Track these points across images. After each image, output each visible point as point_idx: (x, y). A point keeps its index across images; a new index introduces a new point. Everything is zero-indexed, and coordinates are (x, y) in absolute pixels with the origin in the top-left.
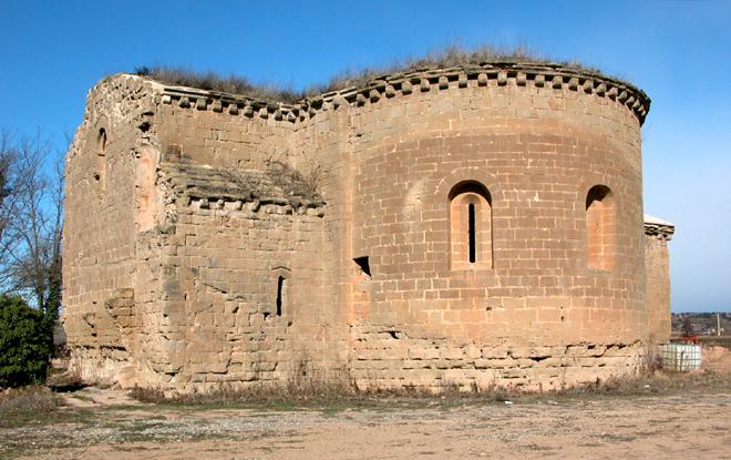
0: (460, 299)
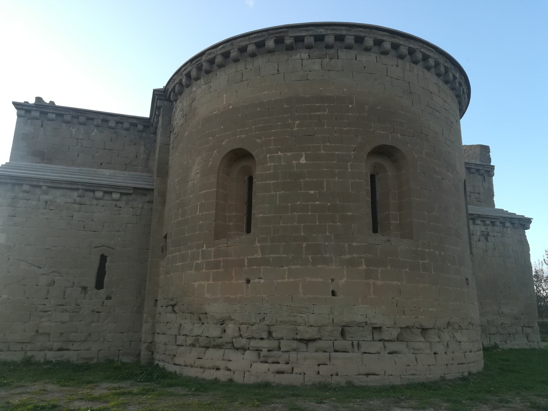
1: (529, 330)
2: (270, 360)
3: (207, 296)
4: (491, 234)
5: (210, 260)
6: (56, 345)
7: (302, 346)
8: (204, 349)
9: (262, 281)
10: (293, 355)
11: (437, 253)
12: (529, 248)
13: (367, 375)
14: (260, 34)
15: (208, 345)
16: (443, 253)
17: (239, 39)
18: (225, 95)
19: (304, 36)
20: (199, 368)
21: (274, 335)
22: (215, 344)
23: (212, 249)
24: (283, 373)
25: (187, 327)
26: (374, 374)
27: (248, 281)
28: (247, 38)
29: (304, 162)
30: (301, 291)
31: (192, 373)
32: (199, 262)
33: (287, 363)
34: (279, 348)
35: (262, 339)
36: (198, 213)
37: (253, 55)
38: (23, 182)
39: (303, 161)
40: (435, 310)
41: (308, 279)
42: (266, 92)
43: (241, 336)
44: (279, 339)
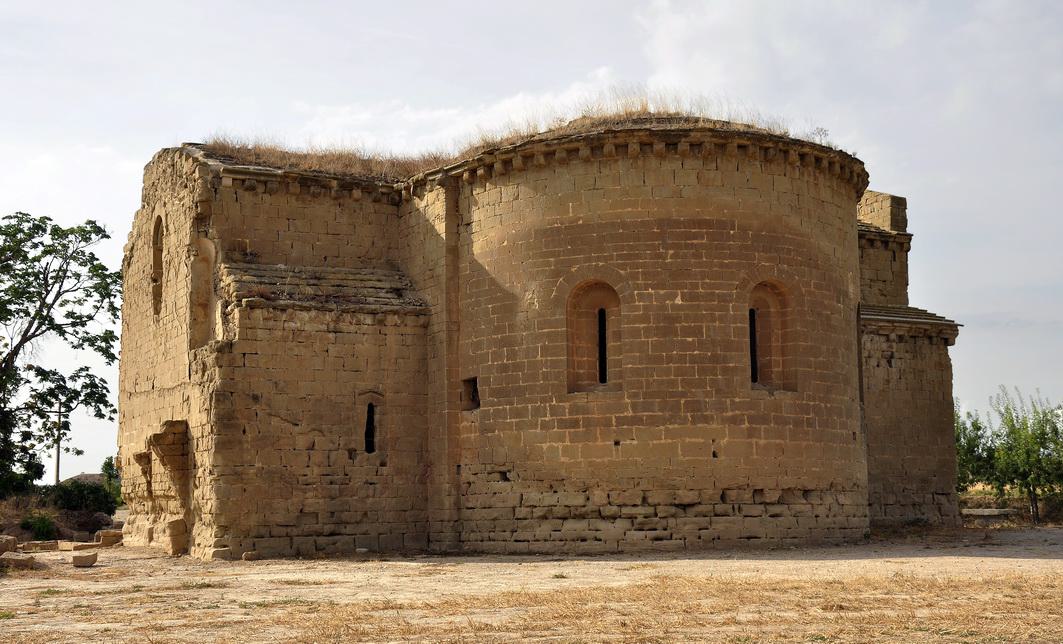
1: (943, 499)
2: (646, 527)
4: (896, 355)
6: (328, 528)
7: (680, 511)
8: (561, 521)
9: (635, 442)
10: (672, 521)
11: (823, 405)
12: (952, 375)
13: (749, 538)
15: (568, 515)
16: (829, 405)
21: (650, 500)
22: (577, 513)
23: (567, 405)
24: (661, 539)
26: (756, 538)
27: (617, 443)
29: (680, 303)
30: (680, 452)
32: (547, 419)
33: (665, 529)
34: (656, 515)
35: (635, 506)
36: (539, 358)
39: (678, 301)
40: (818, 469)
41: (688, 440)
42: (630, 209)
43: (609, 503)
44: (655, 506)
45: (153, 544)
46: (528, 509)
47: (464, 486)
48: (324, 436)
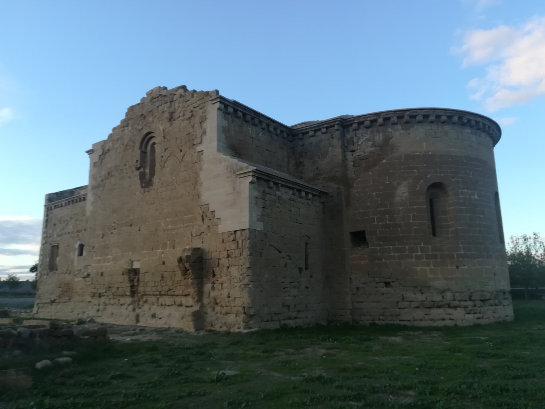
0: (439, 260)
3: (430, 276)
5: (428, 253)
9: (466, 267)
14: (453, 112)
17: (440, 111)
18: (424, 144)
19: (471, 120)
20: (441, 321)
23: (430, 247)
25: (410, 295)
27: (457, 267)
28: (445, 111)
31: (423, 324)
35: (466, 301)
37: (444, 122)
38: (270, 179)
45: (138, 324)
46: (408, 303)
47: (355, 290)
48: (290, 259)
